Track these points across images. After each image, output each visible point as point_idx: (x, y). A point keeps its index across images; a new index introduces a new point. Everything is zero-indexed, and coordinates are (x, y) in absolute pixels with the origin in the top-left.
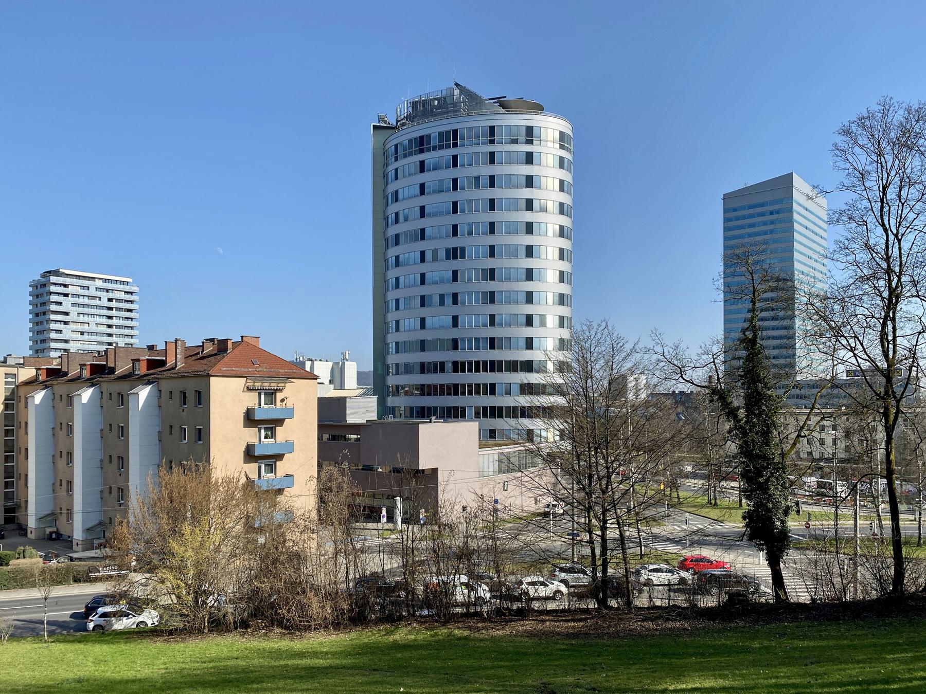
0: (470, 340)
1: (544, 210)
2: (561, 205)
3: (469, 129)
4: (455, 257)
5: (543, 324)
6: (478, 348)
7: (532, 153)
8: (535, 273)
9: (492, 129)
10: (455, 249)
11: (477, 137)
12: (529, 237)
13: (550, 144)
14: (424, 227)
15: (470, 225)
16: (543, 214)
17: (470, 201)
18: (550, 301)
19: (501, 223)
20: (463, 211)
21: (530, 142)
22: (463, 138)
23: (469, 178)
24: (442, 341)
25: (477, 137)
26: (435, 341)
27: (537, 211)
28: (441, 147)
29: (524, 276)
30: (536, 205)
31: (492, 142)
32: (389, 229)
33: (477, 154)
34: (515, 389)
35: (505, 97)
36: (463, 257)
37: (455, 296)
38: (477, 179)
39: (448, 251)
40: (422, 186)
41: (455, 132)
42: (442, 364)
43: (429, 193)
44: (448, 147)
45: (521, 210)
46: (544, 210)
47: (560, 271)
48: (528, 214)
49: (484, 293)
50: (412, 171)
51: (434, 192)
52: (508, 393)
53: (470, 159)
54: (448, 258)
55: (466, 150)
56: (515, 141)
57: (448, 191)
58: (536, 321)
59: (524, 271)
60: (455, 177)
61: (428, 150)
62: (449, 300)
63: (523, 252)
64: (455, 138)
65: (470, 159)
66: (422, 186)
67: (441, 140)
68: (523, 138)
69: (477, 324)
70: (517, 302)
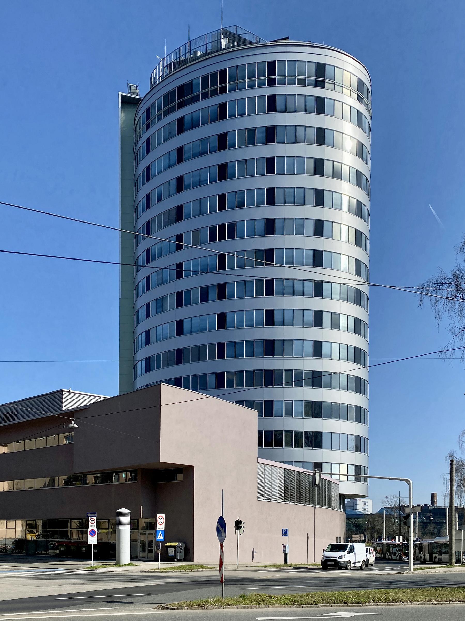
0: (240, 343)
1: (337, 175)
2: (358, 321)
3: (242, 67)
4: (222, 237)
5: (335, 325)
6: (250, 354)
7: (324, 98)
8: (326, 257)
9: (272, 65)
10: (222, 227)
11: (252, 76)
12: (318, 209)
13: (346, 91)
14: (181, 204)
15: (242, 193)
16: (335, 181)
17: (241, 162)
18: (344, 237)
19: (281, 190)
20: (231, 296)
21: (321, 84)
22: (233, 78)
23: (241, 131)
24: (203, 347)
25: (252, 76)
26: (195, 348)
27: (328, 176)
28: (205, 96)
29: (311, 261)
30: (328, 167)
31: (272, 83)
32: (138, 379)
33: (252, 99)
34: (299, 408)
35: (288, 38)
36: (232, 236)
37: (222, 287)
38: (251, 132)
39: (212, 230)
40: (179, 324)
41: (223, 73)
42: (204, 377)
43: (188, 333)
44: (214, 93)
45: (309, 173)
46: (337, 175)
47: (356, 466)
48: (318, 178)
49: (259, 282)
50: (166, 331)
51: (196, 155)
52: (290, 413)
53: (242, 107)
54: (213, 239)
55: (237, 95)
56: (302, 82)
57: (212, 329)
58: (326, 319)
59: (311, 253)
60: (221, 311)
61: (188, 102)
62: (213, 294)
63: (310, 228)
64: (223, 80)
65: (242, 107)
66: (179, 324)
67: (204, 86)
68: (311, 78)
69: (249, 323)
70: (302, 294)
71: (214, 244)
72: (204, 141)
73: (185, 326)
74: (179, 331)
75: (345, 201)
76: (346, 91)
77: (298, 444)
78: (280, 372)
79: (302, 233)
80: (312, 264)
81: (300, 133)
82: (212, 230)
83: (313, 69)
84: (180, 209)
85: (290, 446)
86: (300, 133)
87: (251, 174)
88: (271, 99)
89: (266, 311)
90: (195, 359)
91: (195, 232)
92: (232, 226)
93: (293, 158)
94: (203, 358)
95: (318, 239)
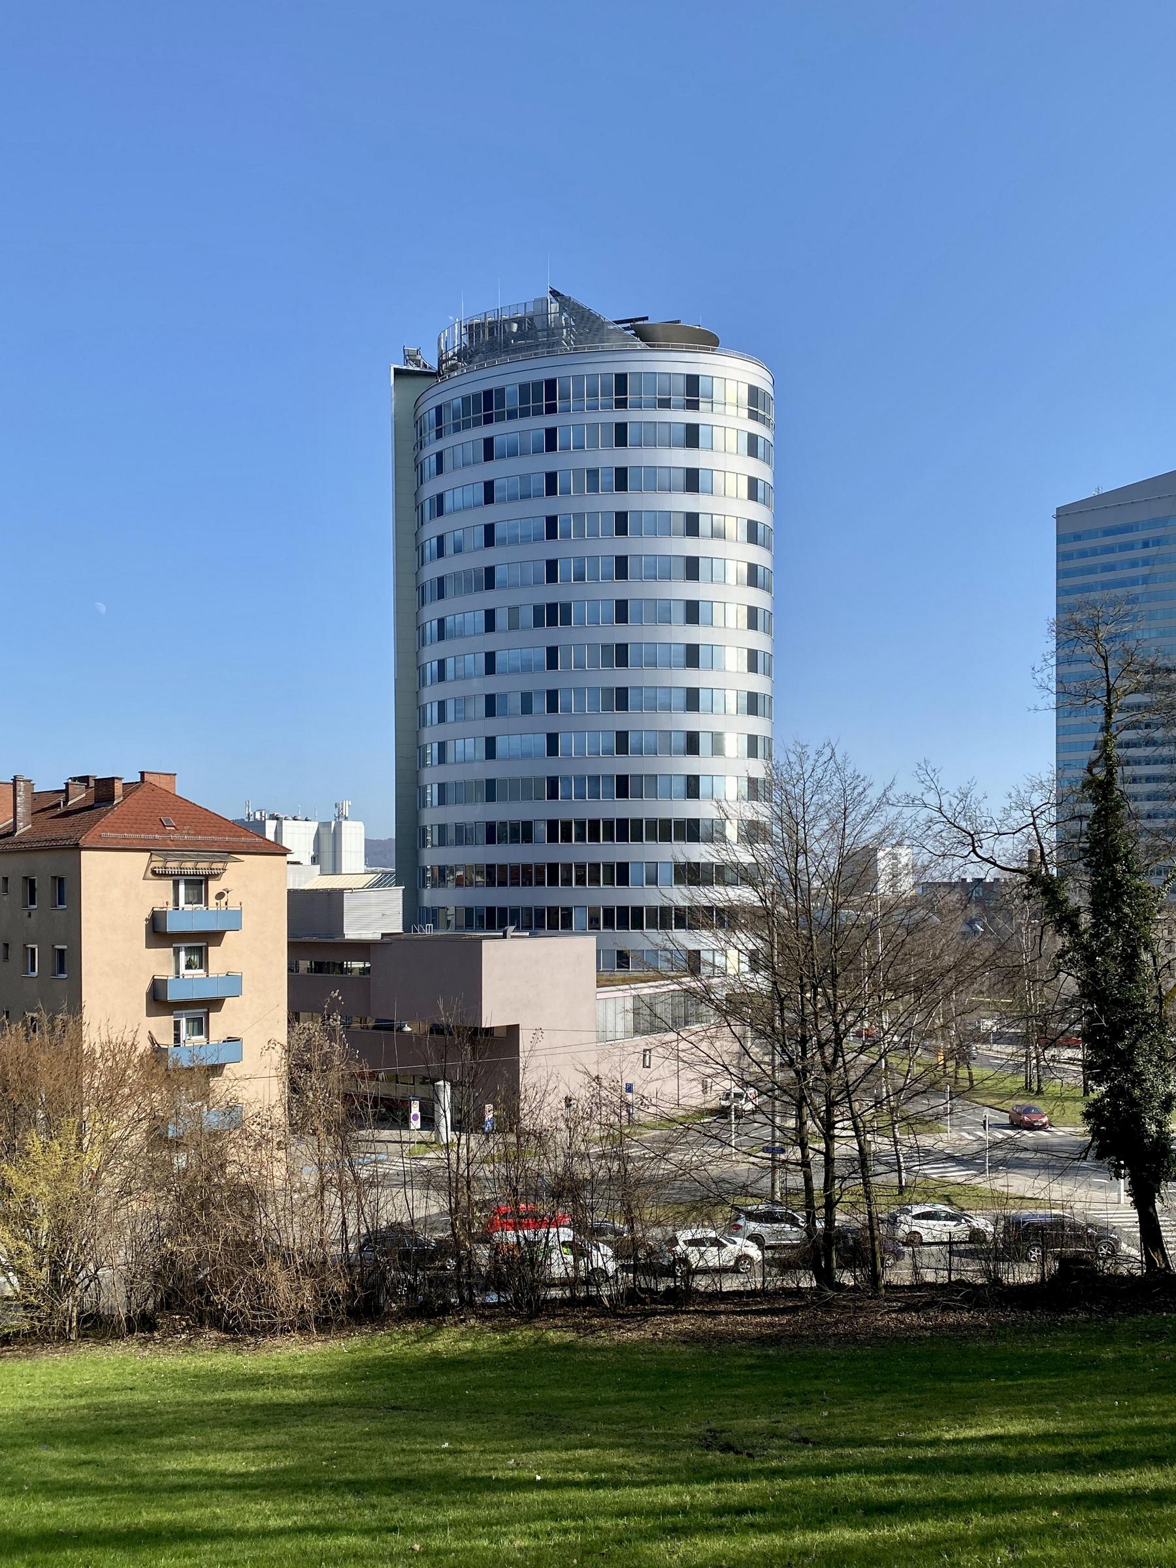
0: (580, 780)
1: (718, 534)
3: (578, 379)
6: (595, 795)
8: (703, 654)
9: (621, 379)
10: (552, 607)
11: (593, 394)
17: (579, 517)
21: (693, 405)
26: (514, 781)
28: (525, 413)
29: (682, 659)
30: (704, 524)
33: (593, 427)
35: (646, 318)
36: (567, 621)
37: (552, 696)
38: (593, 473)
41: (551, 384)
43: (502, 500)
46: (718, 534)
52: (653, 881)
54: (538, 623)
55: (573, 419)
56: (665, 404)
58: (705, 743)
59: (682, 649)
61: (500, 418)
63: (679, 612)
66: (489, 486)
67: (524, 398)
68: (679, 398)
69: (593, 750)
70: (668, 708)
71: (540, 630)
72: (525, 478)
73: (498, 533)
74: (489, 498)
75: (731, 697)
76: (731, 410)
77: (666, 838)
78: (638, 822)
79: (668, 576)
80: (682, 664)
81: (662, 476)
82: (537, 610)
83: (681, 384)
84: (490, 572)
85: (652, 840)
86: (662, 476)
87: (594, 534)
88: (621, 428)
89: (617, 558)
90: (514, 798)
91: (514, 611)
92: (567, 608)
93: (653, 514)
94: (527, 882)
95: (692, 628)
